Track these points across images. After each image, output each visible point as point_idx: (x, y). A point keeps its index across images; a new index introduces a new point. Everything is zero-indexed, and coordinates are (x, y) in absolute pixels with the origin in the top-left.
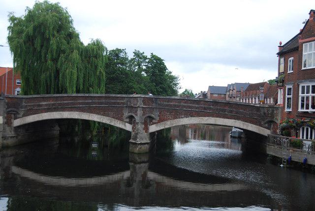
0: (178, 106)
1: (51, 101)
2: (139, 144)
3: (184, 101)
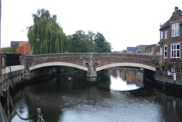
0: (110, 58)
2: (91, 77)
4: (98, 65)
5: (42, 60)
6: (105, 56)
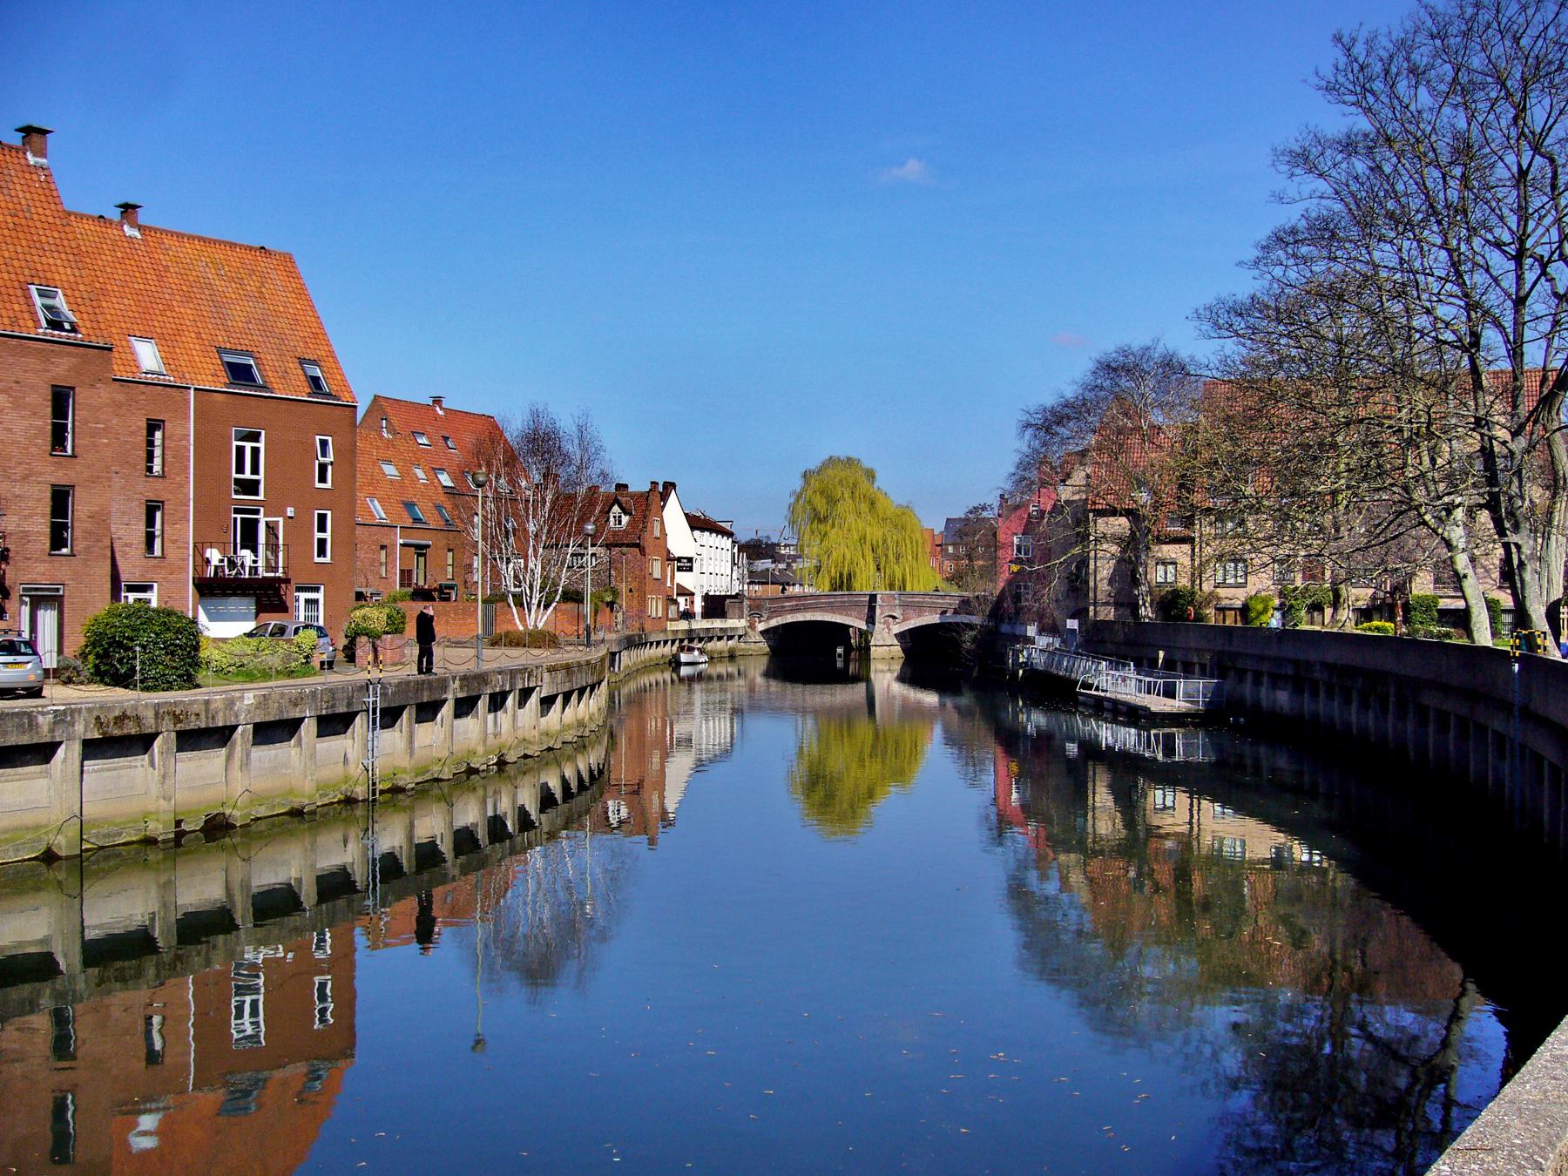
5: (783, 607)
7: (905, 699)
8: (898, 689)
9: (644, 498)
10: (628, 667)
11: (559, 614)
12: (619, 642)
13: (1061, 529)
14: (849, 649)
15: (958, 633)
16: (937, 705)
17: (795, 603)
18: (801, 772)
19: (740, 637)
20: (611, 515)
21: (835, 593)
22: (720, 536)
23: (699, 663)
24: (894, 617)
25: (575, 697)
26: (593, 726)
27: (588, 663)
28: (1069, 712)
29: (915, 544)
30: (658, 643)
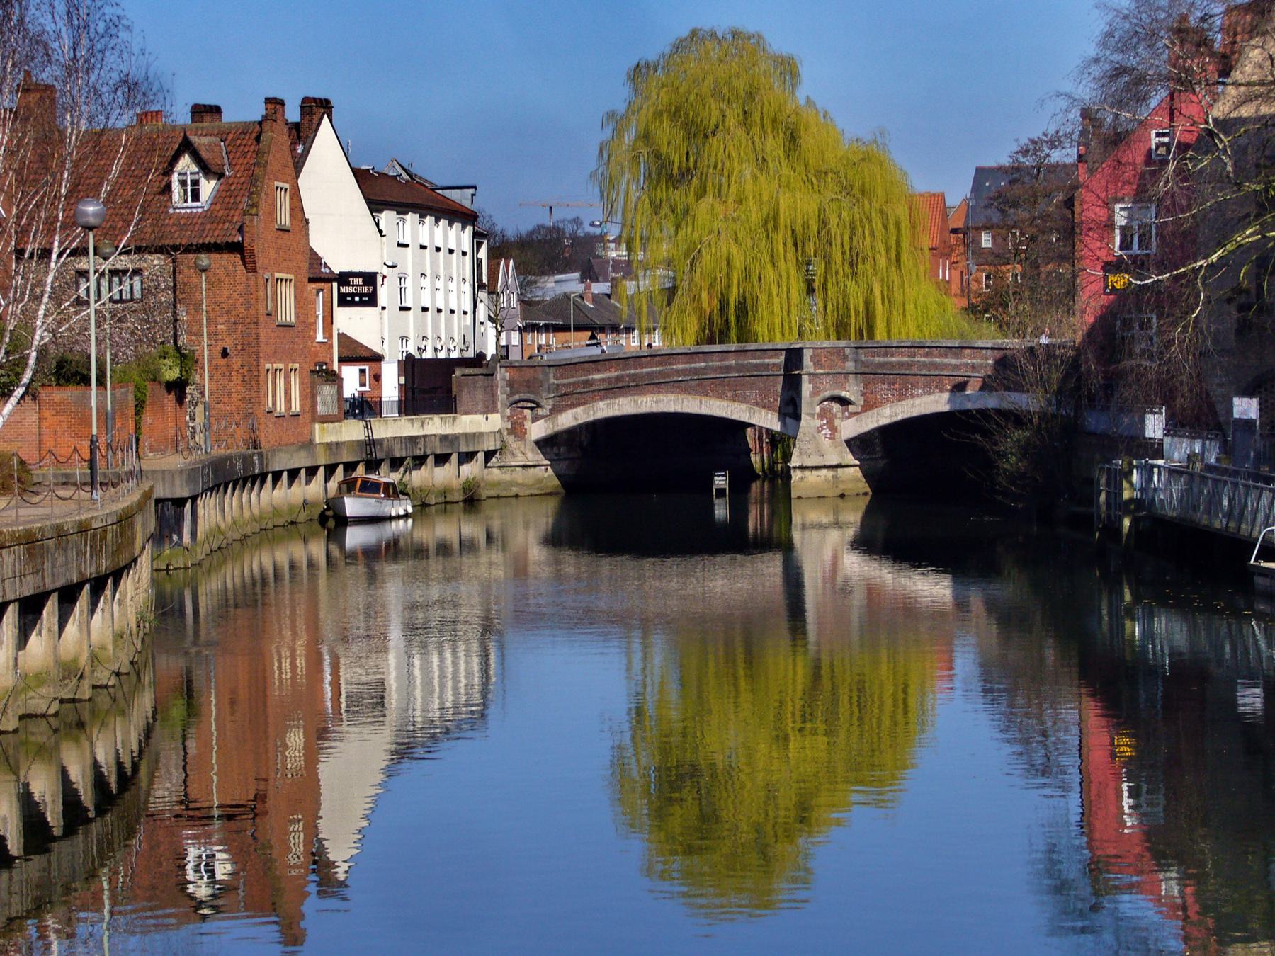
1: (613, 370)
3: (921, 351)
4: (851, 408)
5: (587, 383)
6: (882, 359)
7: (873, 592)
8: (855, 565)
9: (255, 133)
10: (216, 531)
11: (47, 413)
12: (191, 474)
13: (1208, 189)
14: (743, 478)
15: (986, 434)
16: (949, 607)
17: (614, 374)
18: (644, 762)
19: (489, 455)
20: (175, 178)
21: (706, 348)
22: (443, 222)
23: (391, 518)
24: (844, 402)
25: (50, 610)
26: (103, 677)
27: (83, 528)
28: (1237, 614)
29: (892, 228)
30: (293, 474)
